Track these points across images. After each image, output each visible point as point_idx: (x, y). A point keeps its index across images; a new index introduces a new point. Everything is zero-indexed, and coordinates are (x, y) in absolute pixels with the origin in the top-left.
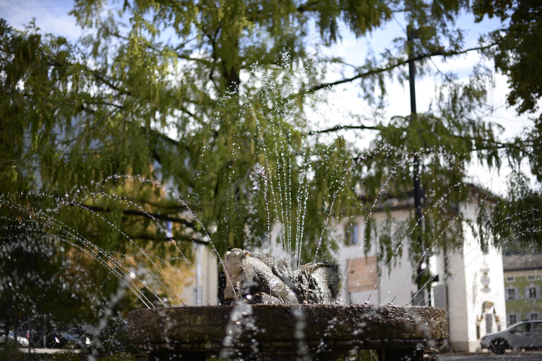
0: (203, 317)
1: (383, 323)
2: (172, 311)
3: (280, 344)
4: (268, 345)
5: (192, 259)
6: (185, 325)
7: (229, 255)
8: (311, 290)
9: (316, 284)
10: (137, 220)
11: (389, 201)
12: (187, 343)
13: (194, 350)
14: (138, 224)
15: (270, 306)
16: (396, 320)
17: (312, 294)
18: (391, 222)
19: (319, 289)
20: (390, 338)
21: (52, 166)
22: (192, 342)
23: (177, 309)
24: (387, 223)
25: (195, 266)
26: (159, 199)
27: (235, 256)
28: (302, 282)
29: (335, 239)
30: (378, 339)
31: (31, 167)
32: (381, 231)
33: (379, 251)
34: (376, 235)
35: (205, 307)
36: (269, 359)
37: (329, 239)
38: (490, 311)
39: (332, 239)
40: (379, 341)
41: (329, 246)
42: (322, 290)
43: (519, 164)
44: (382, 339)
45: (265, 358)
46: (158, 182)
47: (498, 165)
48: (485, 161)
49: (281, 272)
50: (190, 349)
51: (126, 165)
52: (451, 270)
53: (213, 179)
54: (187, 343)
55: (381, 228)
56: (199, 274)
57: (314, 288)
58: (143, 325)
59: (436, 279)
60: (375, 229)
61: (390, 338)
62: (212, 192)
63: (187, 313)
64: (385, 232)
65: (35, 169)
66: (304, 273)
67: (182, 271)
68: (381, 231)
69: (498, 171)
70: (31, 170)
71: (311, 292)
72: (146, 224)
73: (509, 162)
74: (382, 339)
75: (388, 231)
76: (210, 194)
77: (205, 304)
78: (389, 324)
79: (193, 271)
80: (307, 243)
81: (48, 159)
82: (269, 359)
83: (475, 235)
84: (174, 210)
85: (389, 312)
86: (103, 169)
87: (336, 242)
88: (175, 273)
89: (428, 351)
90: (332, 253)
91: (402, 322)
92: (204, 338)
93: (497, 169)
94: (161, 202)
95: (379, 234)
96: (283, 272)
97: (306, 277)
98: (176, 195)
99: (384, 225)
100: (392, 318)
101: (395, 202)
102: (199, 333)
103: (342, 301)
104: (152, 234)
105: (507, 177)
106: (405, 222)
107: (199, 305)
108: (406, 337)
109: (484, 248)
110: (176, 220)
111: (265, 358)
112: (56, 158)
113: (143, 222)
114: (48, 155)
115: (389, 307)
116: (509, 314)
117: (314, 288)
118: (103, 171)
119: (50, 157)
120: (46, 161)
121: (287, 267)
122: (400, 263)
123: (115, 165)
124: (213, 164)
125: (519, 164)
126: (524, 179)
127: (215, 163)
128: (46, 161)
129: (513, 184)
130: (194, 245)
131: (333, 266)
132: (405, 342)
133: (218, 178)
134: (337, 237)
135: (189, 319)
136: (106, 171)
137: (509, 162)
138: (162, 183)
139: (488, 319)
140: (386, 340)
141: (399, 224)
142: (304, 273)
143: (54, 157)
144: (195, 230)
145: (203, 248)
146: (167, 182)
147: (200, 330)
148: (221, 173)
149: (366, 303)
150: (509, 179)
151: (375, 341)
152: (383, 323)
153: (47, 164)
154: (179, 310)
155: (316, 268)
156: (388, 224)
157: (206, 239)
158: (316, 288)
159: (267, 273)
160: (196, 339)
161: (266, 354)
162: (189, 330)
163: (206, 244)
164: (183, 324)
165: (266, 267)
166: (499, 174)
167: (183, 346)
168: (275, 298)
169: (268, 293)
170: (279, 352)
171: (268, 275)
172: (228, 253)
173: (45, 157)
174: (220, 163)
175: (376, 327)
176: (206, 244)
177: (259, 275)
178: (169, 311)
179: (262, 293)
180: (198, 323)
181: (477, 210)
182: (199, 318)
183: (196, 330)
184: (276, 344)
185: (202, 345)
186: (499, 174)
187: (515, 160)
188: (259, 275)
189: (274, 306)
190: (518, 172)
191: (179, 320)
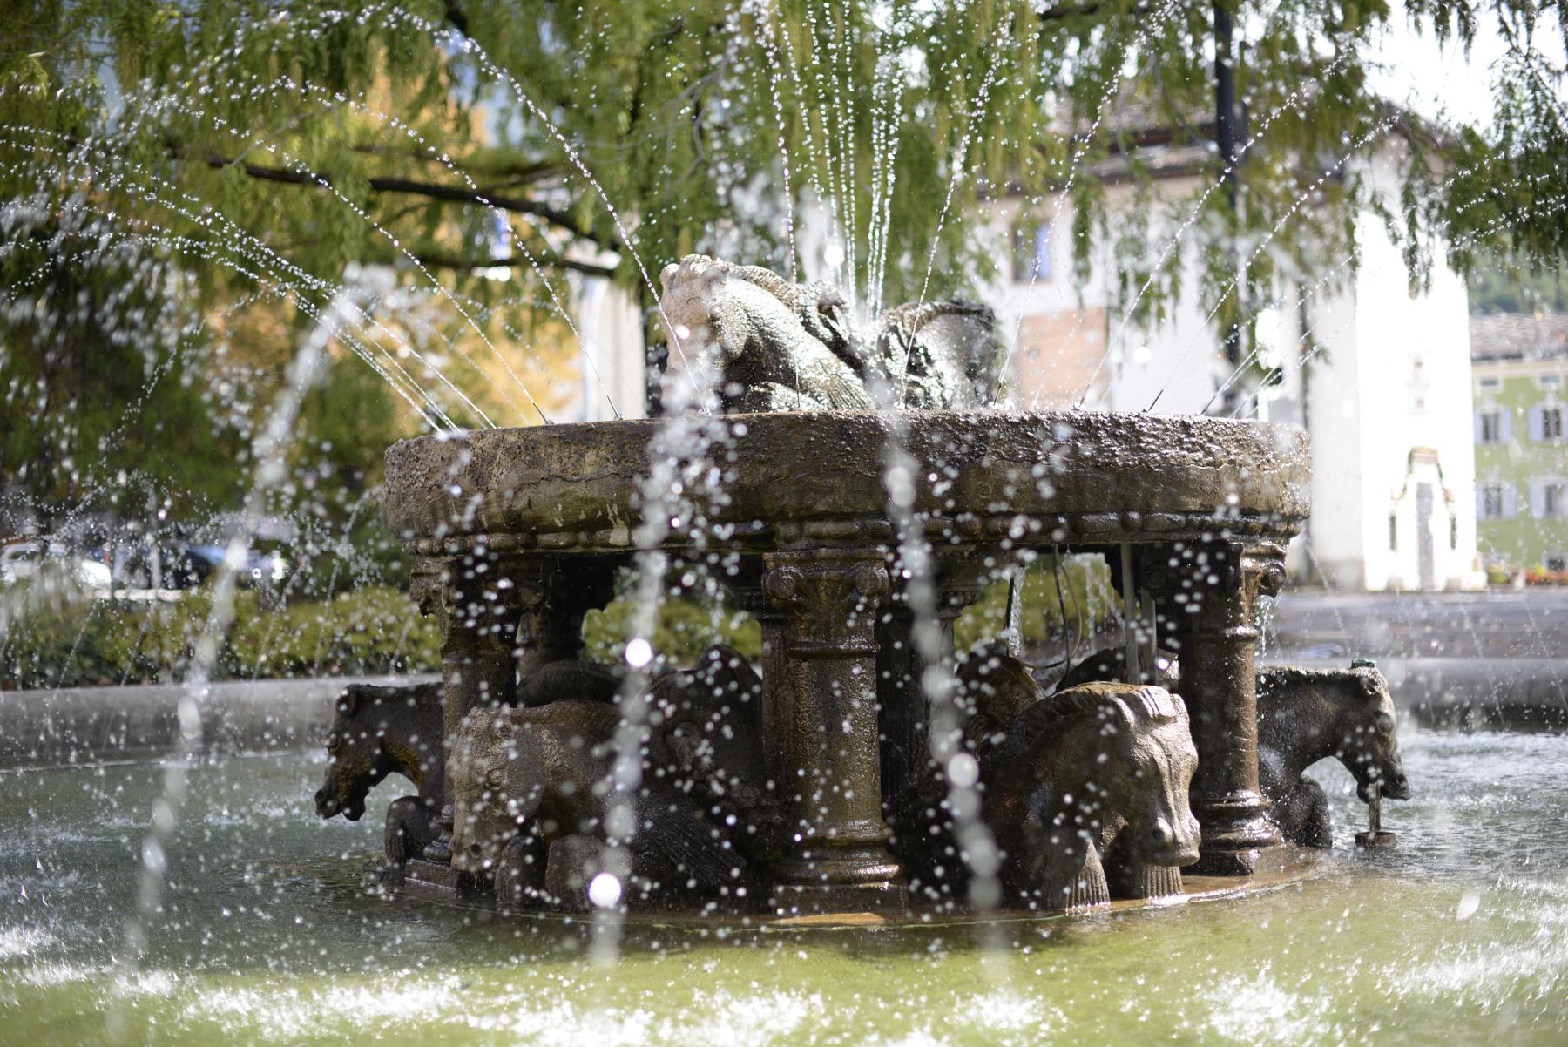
0: (603, 453)
1: (1126, 465)
2: (511, 438)
3: (829, 527)
4: (792, 530)
5: (569, 329)
6: (549, 479)
7: (674, 276)
8: (916, 378)
9: (929, 361)
10: (405, 211)
11: (1142, 154)
12: (554, 529)
13: (578, 550)
14: (409, 219)
15: (796, 417)
16: (1164, 458)
17: (918, 391)
18: (1148, 199)
19: (940, 376)
20: (1145, 511)
21: (147, 47)
22: (573, 527)
23: (525, 432)
24: (1136, 205)
25: (580, 348)
26: (469, 150)
27: (692, 276)
28: (888, 354)
29: (986, 246)
30: (1112, 511)
31: (88, 56)
32: (1121, 227)
33: (1115, 284)
34: (1106, 235)
35: (609, 424)
36: (794, 570)
37: (971, 245)
38: (1424, 473)
39: (980, 247)
40: (1113, 517)
41: (970, 268)
42: (946, 381)
43: (1530, 28)
44: (1123, 512)
45: (783, 569)
46: (467, 98)
47: (1467, 33)
48: (1427, 20)
49: (827, 325)
50: (567, 546)
51: (367, 38)
52: (1321, 337)
53: (624, 77)
54: (554, 529)
55: (1121, 218)
56: (591, 373)
57: (923, 374)
58: (430, 483)
59: (1277, 378)
60: (1103, 221)
61: (1145, 511)
62: (623, 118)
63: (555, 442)
64: (1133, 230)
65: (98, 59)
66: (894, 330)
67: (543, 365)
68: (1121, 227)
69: (1468, 47)
70: (88, 63)
71: (916, 384)
72: (432, 220)
73: (1502, 21)
74: (1123, 512)
75: (1139, 225)
76: (617, 124)
77: (608, 417)
78: (1145, 470)
79: (574, 364)
80: (905, 261)
81: (137, 25)
82: (794, 570)
83: (1395, 239)
84: (514, 178)
85: (1143, 434)
86: (300, 52)
87: (992, 256)
88: (522, 371)
89: (1254, 550)
90: (982, 287)
91: (1180, 464)
92: (605, 515)
93: (1462, 43)
94: (473, 156)
95: (1116, 235)
96: (833, 323)
97: (902, 343)
98: (517, 130)
99: (1130, 208)
100: (1153, 451)
101: (1159, 156)
102: (592, 500)
103: (1008, 407)
104: (453, 254)
105: (1492, 67)
106: (1189, 200)
107: (592, 419)
108: (1192, 508)
109: (1418, 284)
110: (518, 207)
111: (783, 569)
112: (159, 24)
113: (422, 212)
114: (135, 15)
115: (1144, 420)
116: (1482, 486)
117: (923, 374)
118: (300, 58)
119: (142, 21)
120: (130, 30)
121: (844, 310)
122: (1174, 319)
123: (337, 38)
124: (625, 32)
125: (1530, 28)
126: (1543, 74)
127: (631, 27)
128: (130, 30)
129: (1509, 89)
130: (574, 279)
131: (979, 313)
132: (1189, 523)
133: (640, 71)
134: (992, 241)
135: (560, 460)
136: (312, 57)
137: (1502, 21)
138: (477, 93)
139: (1423, 493)
140: (1135, 516)
141: (1171, 205)
142: (894, 330)
143: (155, 20)
144: (578, 234)
145: (600, 287)
146: (490, 96)
147: (594, 492)
148: (648, 65)
149: (1076, 410)
150: (1498, 72)
151: (1103, 518)
152: (1126, 465)
153: (132, 36)
154: (532, 436)
155: (930, 317)
156: (1142, 206)
157: (611, 260)
158: (930, 371)
159: (787, 328)
160: (582, 517)
161: (785, 555)
162: (562, 491)
163: (609, 274)
164: (543, 474)
165: (785, 311)
166: (1467, 60)
167: (546, 538)
168: (812, 401)
169: (793, 387)
170: (823, 550)
171: (788, 334)
172: (672, 268)
173: (127, 18)
174: (644, 29)
175: (1108, 477)
176: (609, 274)
177: (761, 332)
178: (503, 440)
179: (771, 384)
180: (588, 471)
181: (1401, 163)
182: (590, 457)
183: (581, 490)
184: (813, 527)
185: (600, 534)
186: (1467, 60)
187: (1519, 15)
188: (761, 332)
189: (808, 418)
190: (1524, 49)
191: (535, 463)
